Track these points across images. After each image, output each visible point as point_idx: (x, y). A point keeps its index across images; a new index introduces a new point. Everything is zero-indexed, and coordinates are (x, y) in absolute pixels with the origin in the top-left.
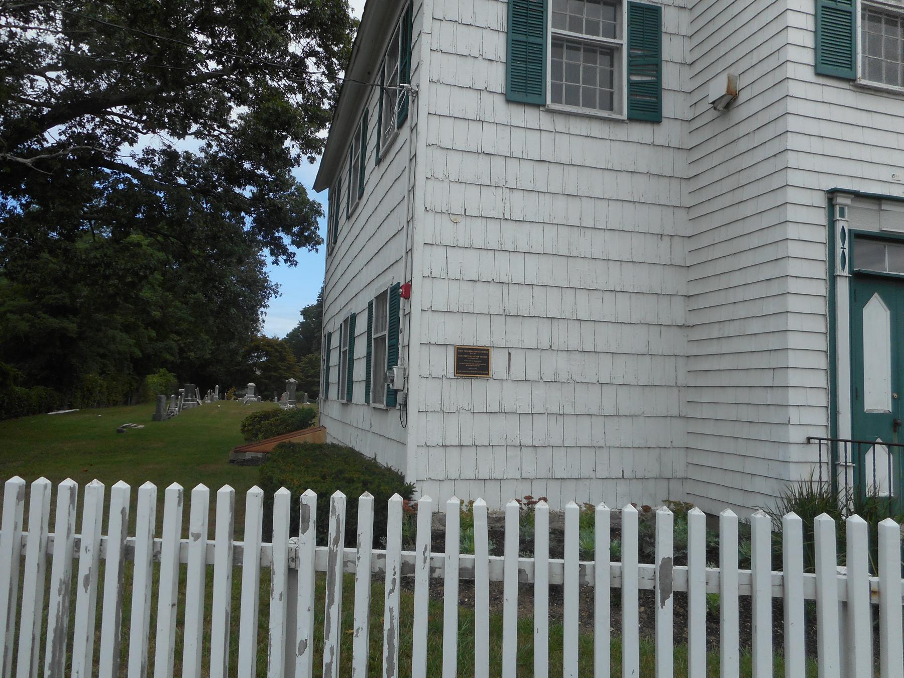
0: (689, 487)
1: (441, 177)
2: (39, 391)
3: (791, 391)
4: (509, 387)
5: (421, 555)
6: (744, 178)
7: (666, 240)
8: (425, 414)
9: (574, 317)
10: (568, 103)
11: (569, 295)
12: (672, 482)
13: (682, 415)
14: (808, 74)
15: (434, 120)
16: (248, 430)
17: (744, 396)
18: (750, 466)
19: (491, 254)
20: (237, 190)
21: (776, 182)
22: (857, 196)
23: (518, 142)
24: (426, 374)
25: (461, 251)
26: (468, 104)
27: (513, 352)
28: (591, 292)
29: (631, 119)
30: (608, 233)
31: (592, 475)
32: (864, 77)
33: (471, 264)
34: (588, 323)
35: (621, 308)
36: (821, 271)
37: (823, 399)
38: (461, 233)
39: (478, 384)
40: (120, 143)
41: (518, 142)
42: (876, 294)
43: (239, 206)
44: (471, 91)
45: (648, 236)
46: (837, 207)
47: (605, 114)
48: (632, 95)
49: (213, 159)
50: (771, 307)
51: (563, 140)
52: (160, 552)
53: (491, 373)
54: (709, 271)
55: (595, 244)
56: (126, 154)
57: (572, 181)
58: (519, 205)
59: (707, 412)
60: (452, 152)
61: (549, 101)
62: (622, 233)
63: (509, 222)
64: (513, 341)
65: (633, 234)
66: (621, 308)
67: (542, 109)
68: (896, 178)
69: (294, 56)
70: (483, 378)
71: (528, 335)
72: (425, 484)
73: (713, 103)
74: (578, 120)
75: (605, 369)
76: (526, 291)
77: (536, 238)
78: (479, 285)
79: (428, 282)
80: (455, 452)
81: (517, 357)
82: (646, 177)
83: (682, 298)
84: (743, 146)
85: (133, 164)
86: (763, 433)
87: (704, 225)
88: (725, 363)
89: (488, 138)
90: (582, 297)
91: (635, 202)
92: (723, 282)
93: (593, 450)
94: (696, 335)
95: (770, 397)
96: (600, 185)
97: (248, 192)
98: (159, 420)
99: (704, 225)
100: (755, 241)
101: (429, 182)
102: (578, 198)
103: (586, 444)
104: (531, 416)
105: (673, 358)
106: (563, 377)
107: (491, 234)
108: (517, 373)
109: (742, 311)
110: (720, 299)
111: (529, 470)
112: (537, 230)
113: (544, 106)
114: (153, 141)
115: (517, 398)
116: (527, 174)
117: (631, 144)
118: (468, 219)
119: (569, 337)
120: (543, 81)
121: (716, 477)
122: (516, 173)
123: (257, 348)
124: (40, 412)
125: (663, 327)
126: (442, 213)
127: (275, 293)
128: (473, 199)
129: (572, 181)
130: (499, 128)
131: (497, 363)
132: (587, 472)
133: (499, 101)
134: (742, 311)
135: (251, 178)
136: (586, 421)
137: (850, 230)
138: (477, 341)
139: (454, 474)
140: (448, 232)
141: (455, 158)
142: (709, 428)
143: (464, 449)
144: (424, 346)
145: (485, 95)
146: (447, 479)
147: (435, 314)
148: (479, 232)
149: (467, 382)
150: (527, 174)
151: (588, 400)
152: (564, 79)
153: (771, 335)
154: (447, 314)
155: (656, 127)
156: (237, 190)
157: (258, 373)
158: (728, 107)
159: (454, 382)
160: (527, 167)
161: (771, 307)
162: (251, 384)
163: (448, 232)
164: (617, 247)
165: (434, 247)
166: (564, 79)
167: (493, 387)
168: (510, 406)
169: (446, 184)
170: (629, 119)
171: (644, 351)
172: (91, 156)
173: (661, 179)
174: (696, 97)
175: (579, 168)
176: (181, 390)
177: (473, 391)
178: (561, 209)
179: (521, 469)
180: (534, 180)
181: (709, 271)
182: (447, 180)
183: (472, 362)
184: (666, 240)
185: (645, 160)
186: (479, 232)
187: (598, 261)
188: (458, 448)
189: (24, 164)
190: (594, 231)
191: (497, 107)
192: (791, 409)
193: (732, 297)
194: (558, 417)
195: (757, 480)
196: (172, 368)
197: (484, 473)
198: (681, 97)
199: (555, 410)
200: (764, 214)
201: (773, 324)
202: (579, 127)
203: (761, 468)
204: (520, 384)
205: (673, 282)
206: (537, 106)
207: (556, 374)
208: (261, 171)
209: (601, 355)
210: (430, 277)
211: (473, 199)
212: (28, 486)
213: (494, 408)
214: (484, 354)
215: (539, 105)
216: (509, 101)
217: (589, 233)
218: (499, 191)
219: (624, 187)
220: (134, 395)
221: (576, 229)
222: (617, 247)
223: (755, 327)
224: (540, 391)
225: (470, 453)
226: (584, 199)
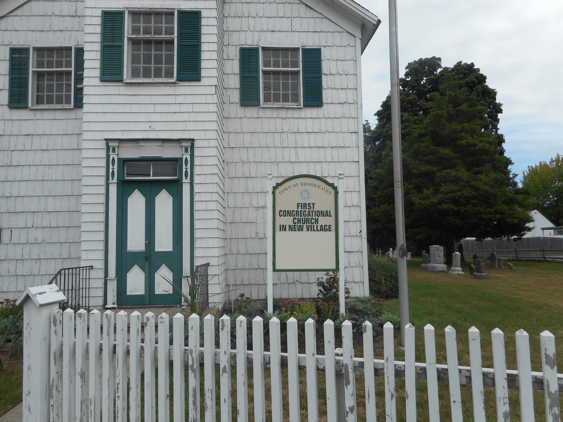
5: (389, 364)
14: (97, 81)
22: (120, 141)
32: (127, 78)
34: (54, 213)
36: (103, 181)
37: (101, 246)
42: (137, 190)
46: (111, 148)
52: (269, 363)
64: (13, 224)
68: (152, 128)
71: (21, 221)
81: (15, 233)
106: (40, 240)
108: (15, 240)
133: (6, 109)
137: (119, 159)
170: (74, 107)
202: (59, 115)
207: (36, 239)
212: (129, 316)
215: (26, 108)
217: (55, 167)
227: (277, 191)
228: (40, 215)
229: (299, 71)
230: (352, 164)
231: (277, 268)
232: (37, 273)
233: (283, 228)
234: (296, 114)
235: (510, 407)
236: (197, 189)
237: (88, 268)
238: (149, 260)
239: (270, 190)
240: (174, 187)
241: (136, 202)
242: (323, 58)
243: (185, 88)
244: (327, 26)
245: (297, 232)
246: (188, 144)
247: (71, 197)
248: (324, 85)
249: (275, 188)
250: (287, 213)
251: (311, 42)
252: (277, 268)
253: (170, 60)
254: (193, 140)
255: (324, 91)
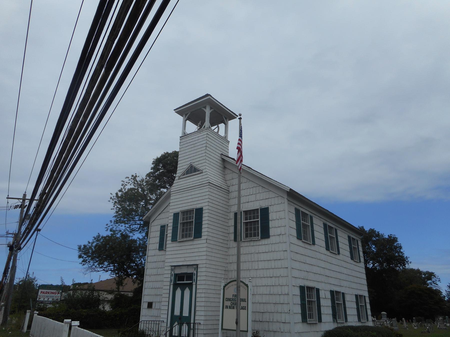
32: (179, 239)
133: (158, 251)
137: (174, 274)
227: (225, 288)
229: (258, 221)
230: (285, 269)
231: (224, 328)
233: (227, 307)
234: (258, 243)
236: (198, 287)
237: (148, 322)
238: (243, 308)
239: (222, 287)
240: (190, 286)
241: (179, 292)
242: (270, 212)
243: (197, 241)
244: (272, 195)
245: (232, 310)
246: (195, 266)
248: (270, 226)
249: (224, 287)
250: (229, 300)
251: (264, 204)
252: (224, 328)
253: (190, 230)
254: (197, 265)
255: (270, 230)
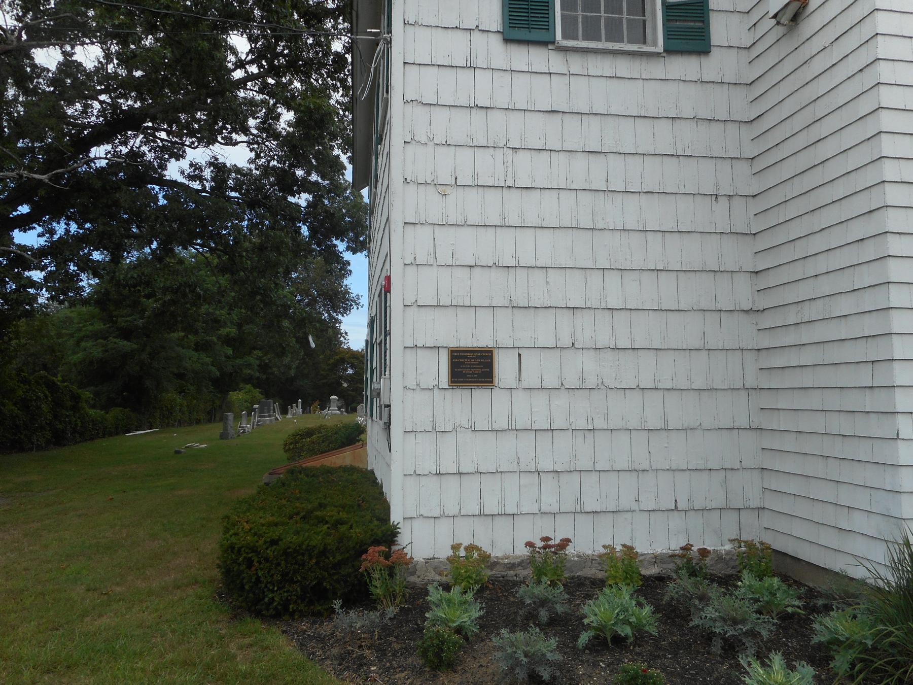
0: (767, 520)
1: (424, 139)
2: (116, 412)
3: (898, 392)
4: (520, 397)
6: (821, 109)
7: (723, 201)
8: (413, 435)
9: (603, 306)
10: (586, 38)
11: (595, 279)
12: (743, 513)
13: (753, 426)
15: (412, 71)
16: (289, 449)
17: (834, 401)
18: (845, 497)
19: (491, 231)
20: (291, 199)
21: (864, 106)
23: (521, 91)
24: (412, 384)
25: (452, 230)
26: (454, 47)
27: (524, 353)
28: (624, 273)
29: (670, 51)
30: (644, 196)
31: (635, 506)
33: (467, 247)
34: (623, 313)
35: (667, 292)
38: (455, 206)
39: (480, 395)
40: (167, 160)
41: (521, 91)
43: (294, 214)
44: (459, 33)
45: (698, 198)
47: (634, 47)
48: (668, 20)
49: (266, 170)
50: (867, 277)
51: (579, 84)
53: (496, 380)
54: (781, 236)
55: (630, 212)
56: (174, 171)
57: (594, 134)
58: (526, 169)
59: (785, 422)
60: (437, 109)
61: (559, 36)
62: (663, 196)
63: (513, 191)
64: (524, 339)
65: (678, 196)
66: (667, 292)
67: (550, 47)
69: (337, 54)
70: (486, 388)
71: (543, 330)
72: (416, 523)
73: (775, 16)
74: (599, 57)
75: (646, 371)
76: (539, 276)
77: (549, 208)
78: (477, 271)
79: (410, 270)
80: (453, 482)
81: (530, 361)
82: (693, 124)
83: (748, 275)
84: (818, 65)
85: (181, 179)
86: (862, 451)
87: (772, 178)
88: (806, 357)
89: (483, 87)
90: (613, 279)
91: (678, 156)
92: (799, 251)
93: (635, 474)
94: (768, 321)
95: (869, 402)
96: (629, 136)
97: (303, 200)
98: (226, 439)
99: (772, 178)
100: (839, 190)
101: (408, 147)
102: (602, 156)
103: (625, 466)
104: (550, 433)
105: (739, 353)
106: (591, 382)
107: (491, 207)
108: (530, 378)
109: (825, 286)
110: (797, 272)
111: (550, 502)
112: (550, 198)
113: (553, 43)
114: (199, 155)
115: (529, 410)
116: (534, 130)
117: (671, 83)
118: (461, 190)
119: (599, 331)
120: (551, 12)
121: (801, 509)
122: (517, 129)
123: (342, 361)
124: (117, 434)
125: (722, 313)
126: (426, 183)
127: (357, 304)
128: (464, 164)
129: (594, 134)
130: (497, 75)
131: (504, 367)
132: (627, 502)
133: (496, 42)
134: (825, 286)
135: (305, 185)
136: (624, 437)
138: (477, 340)
139: (452, 510)
140: (433, 206)
141: (440, 115)
142: (789, 444)
143: (464, 477)
144: (408, 351)
145: (476, 35)
146: (443, 516)
147: (423, 309)
148: (474, 205)
149: (466, 393)
150: (534, 130)
151: (626, 410)
152: (580, 8)
153: (867, 314)
154: (437, 309)
155: (704, 59)
156: (291, 199)
157: (345, 385)
158: (796, 18)
159: (449, 394)
160: (535, 120)
161: (867, 277)
162: (334, 397)
163: (433, 206)
164: (656, 214)
165: (418, 227)
166: (580, 8)
167: (499, 398)
168: (522, 422)
169: (430, 148)
171: (697, 344)
172: (141, 174)
173: (713, 124)
174: (755, 17)
175: (603, 117)
176: (255, 406)
177: (474, 403)
178: (581, 171)
179: (539, 501)
180: (544, 135)
181: (781, 236)
182: (432, 143)
183: (471, 368)
184: (723, 201)
185: (690, 101)
186: (474, 205)
187: (631, 233)
188: (457, 477)
189: (41, 180)
190: (625, 195)
191: (494, 50)
192: (900, 418)
193: (812, 268)
194: (586, 432)
195: (857, 515)
196: (258, 384)
197: (492, 507)
198: (736, 18)
199: (582, 424)
200: (850, 152)
201: (869, 301)
203: (861, 500)
204: (535, 392)
205: (736, 255)
206: (544, 44)
207: (582, 379)
208: (314, 177)
209: (640, 352)
210: (415, 264)
211: (464, 164)
213: (502, 424)
214: (486, 357)
216: (507, 41)
217: (618, 198)
218: (499, 152)
219: (664, 137)
220: (214, 414)
221: (601, 194)
222: (656, 214)
223: (845, 306)
224: (561, 401)
225: (472, 483)
226: (610, 156)
228: (588, 316)
232: (589, 466)
235: (162, 206)
247: (663, 275)
